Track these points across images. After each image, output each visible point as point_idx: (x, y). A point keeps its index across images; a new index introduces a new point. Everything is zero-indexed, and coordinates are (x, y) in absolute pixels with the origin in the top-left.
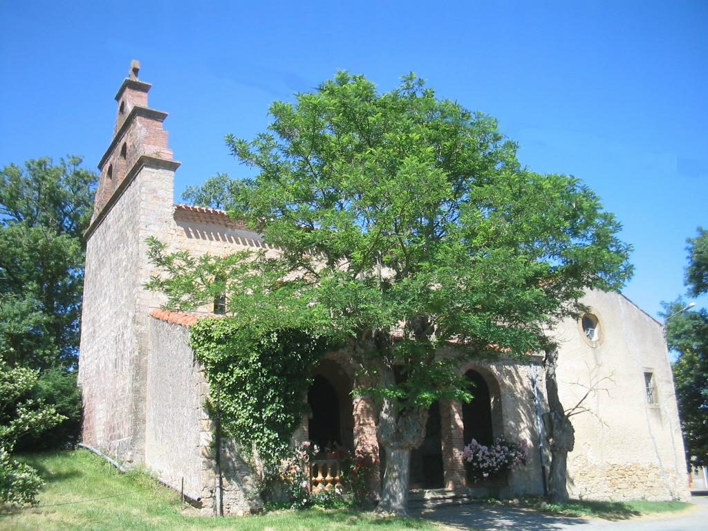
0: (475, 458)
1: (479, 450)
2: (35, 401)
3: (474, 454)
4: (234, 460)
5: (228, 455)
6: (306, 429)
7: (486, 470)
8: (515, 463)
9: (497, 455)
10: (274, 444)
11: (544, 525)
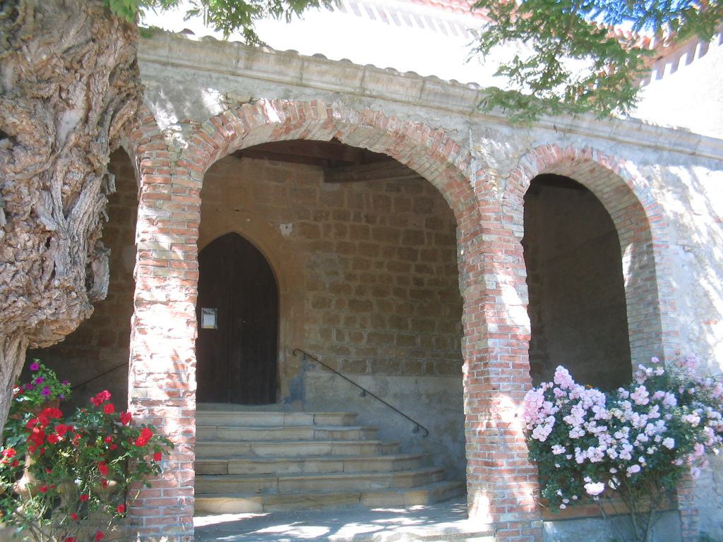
0: (561, 429)
1: (576, 401)
3: (559, 416)
7: (602, 469)
8: (700, 448)
9: (638, 420)
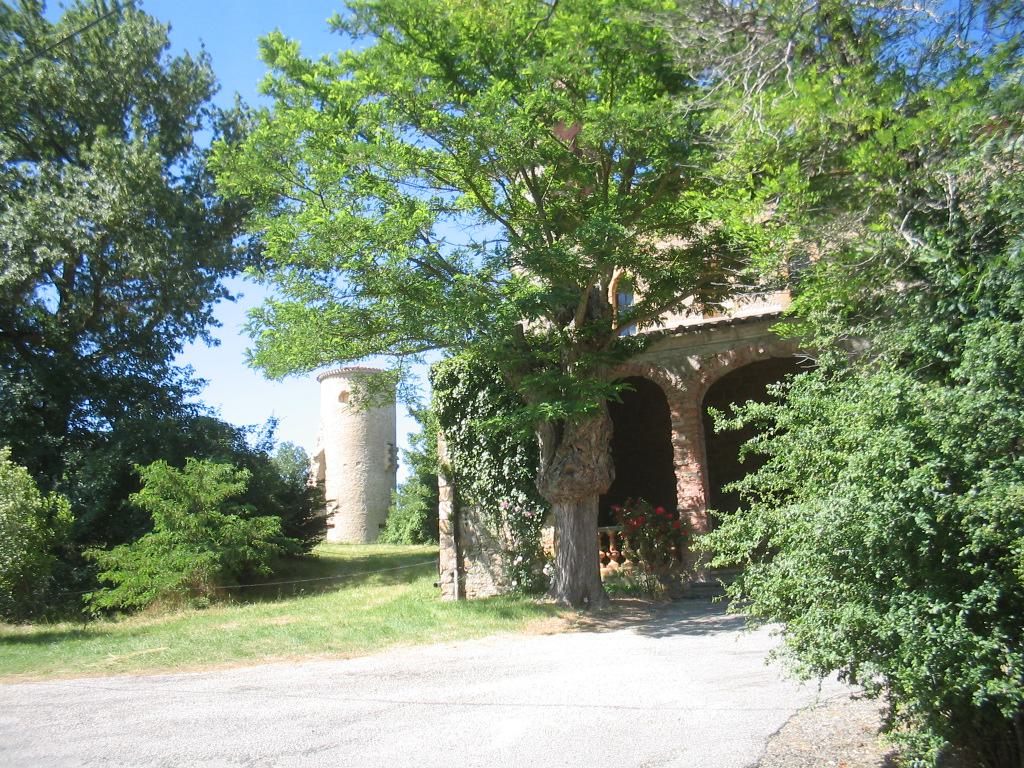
2: (905, 536)
4: (478, 534)
5: (471, 528)
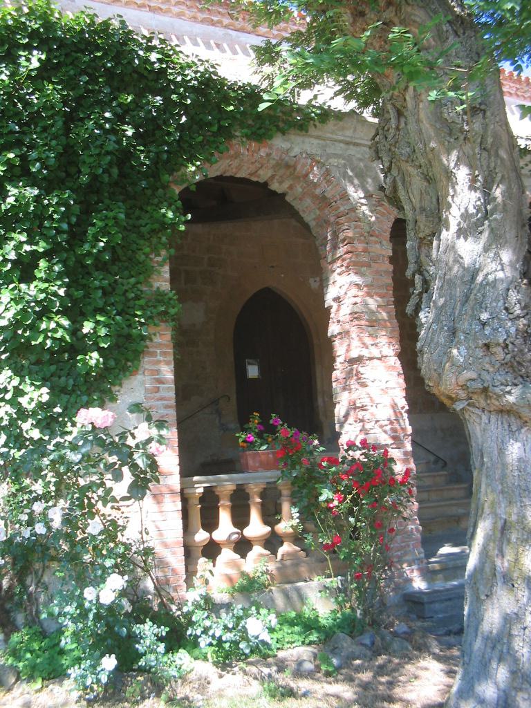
6: (168, 372)
10: (37, 425)
11: (431, 560)
